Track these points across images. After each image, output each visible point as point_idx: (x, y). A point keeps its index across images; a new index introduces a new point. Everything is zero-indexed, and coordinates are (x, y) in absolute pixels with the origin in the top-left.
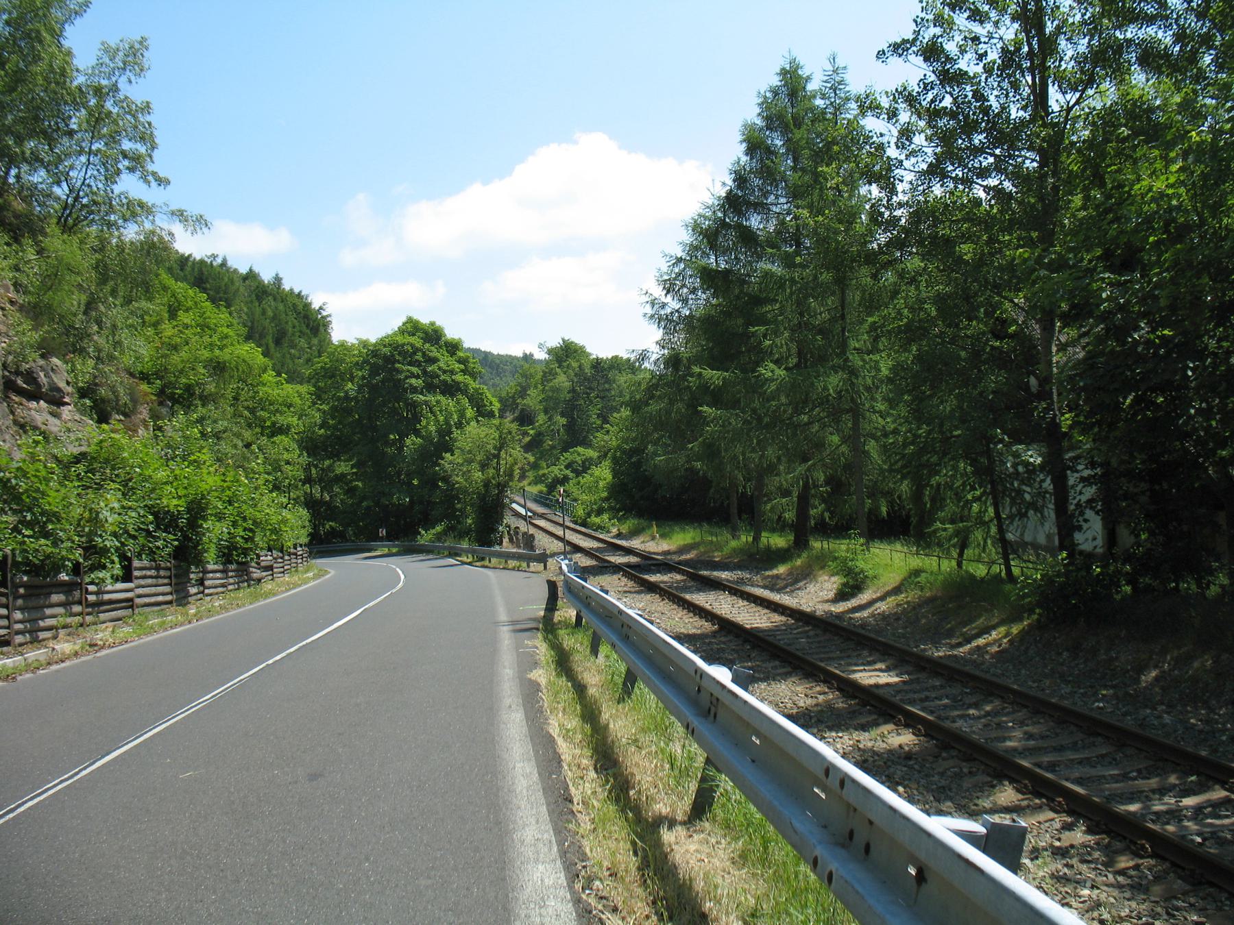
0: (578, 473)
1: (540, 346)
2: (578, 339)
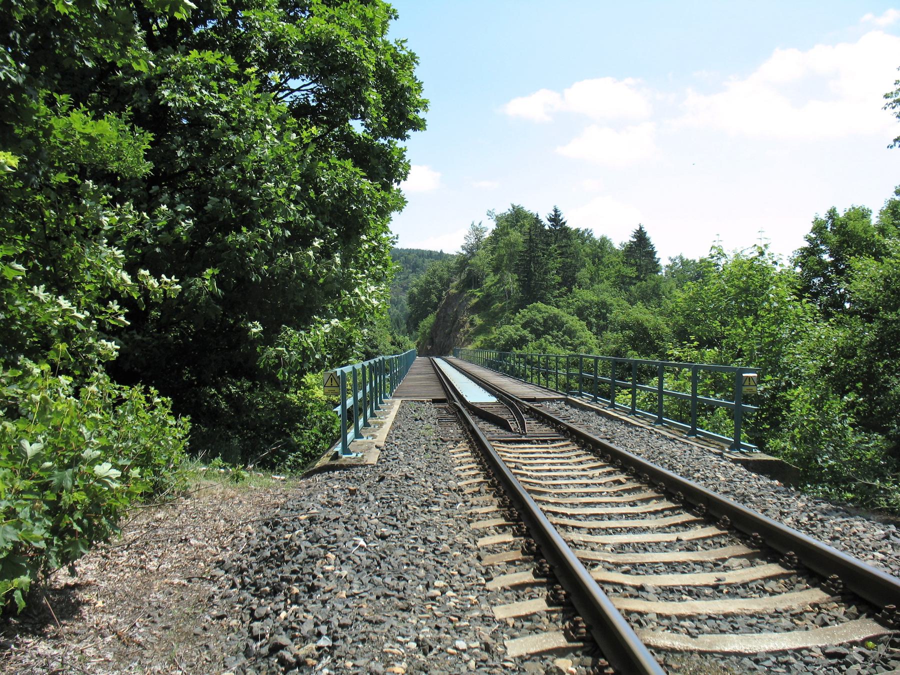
0: (538, 335)
1: (490, 214)
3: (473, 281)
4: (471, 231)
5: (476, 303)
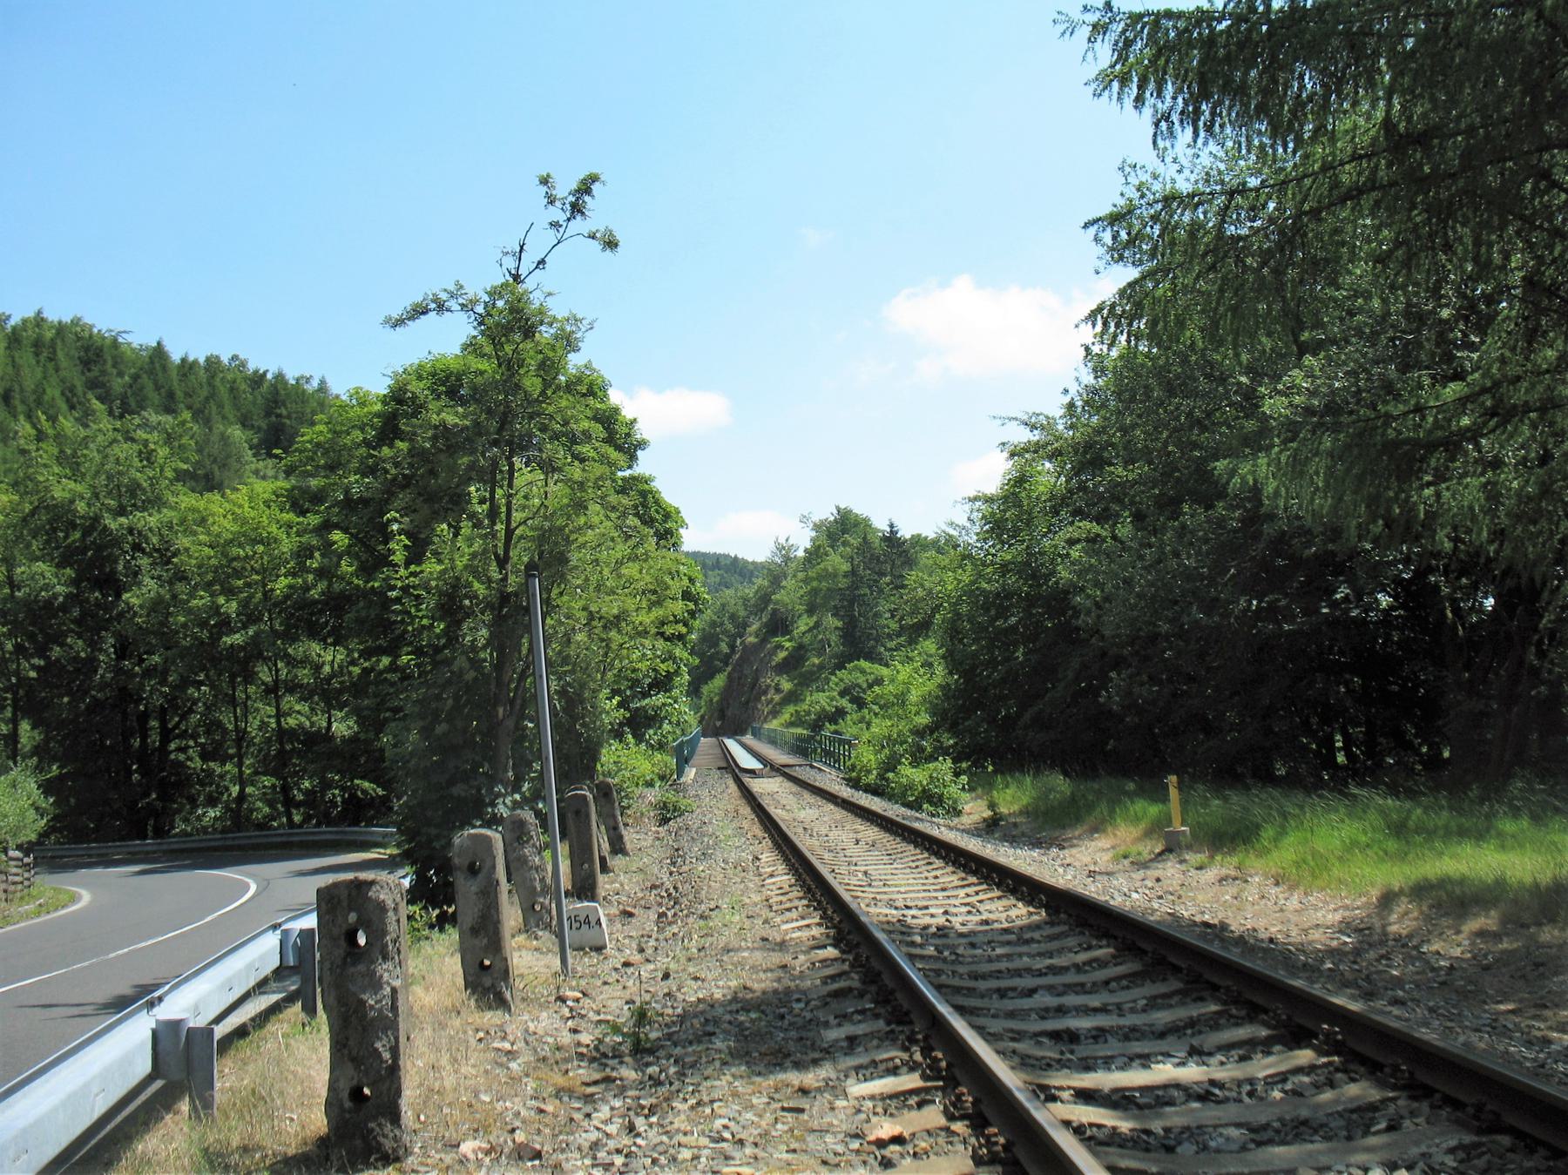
1: (804, 519)
2: (860, 509)
3: (779, 625)
4: (775, 550)
5: (785, 659)
